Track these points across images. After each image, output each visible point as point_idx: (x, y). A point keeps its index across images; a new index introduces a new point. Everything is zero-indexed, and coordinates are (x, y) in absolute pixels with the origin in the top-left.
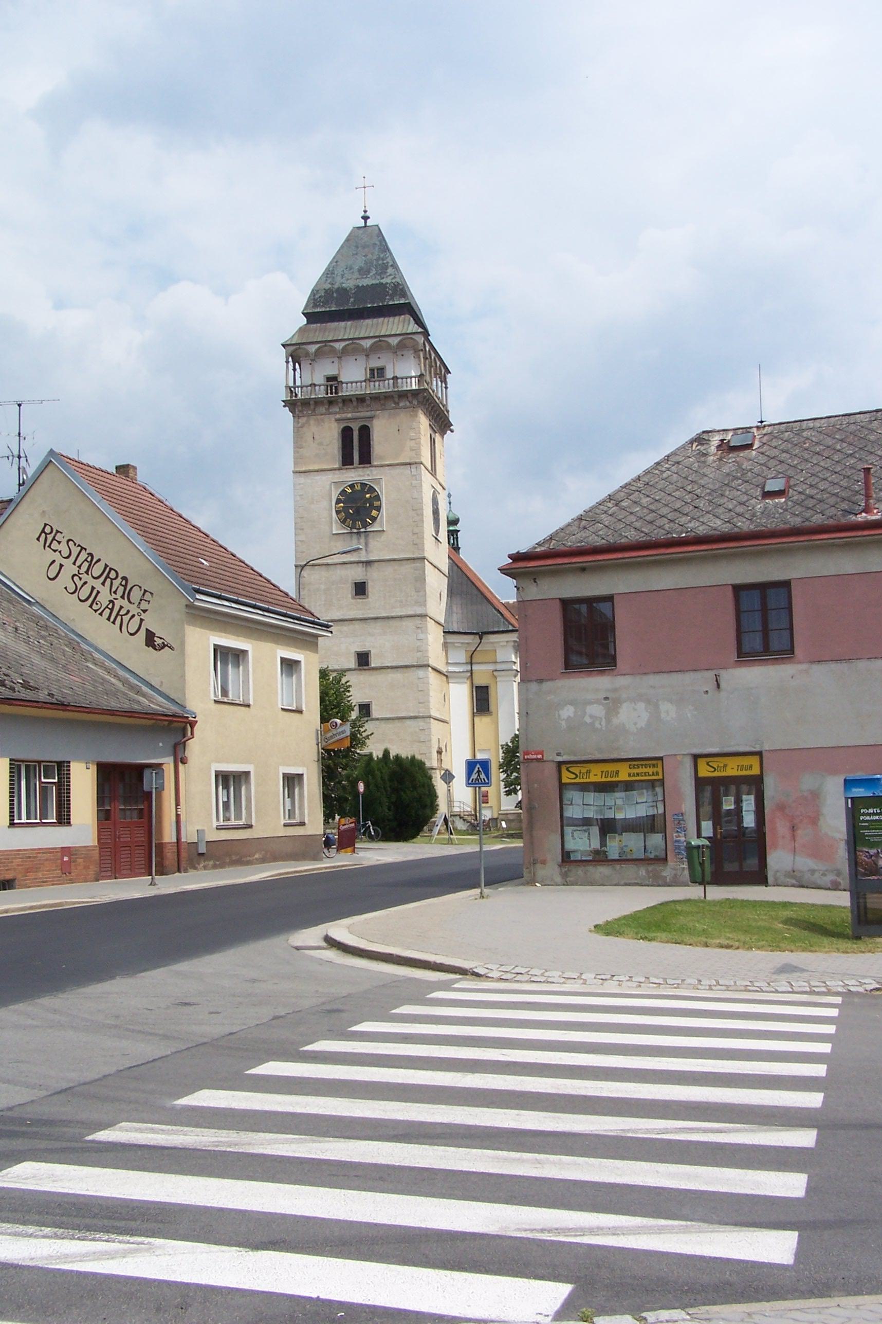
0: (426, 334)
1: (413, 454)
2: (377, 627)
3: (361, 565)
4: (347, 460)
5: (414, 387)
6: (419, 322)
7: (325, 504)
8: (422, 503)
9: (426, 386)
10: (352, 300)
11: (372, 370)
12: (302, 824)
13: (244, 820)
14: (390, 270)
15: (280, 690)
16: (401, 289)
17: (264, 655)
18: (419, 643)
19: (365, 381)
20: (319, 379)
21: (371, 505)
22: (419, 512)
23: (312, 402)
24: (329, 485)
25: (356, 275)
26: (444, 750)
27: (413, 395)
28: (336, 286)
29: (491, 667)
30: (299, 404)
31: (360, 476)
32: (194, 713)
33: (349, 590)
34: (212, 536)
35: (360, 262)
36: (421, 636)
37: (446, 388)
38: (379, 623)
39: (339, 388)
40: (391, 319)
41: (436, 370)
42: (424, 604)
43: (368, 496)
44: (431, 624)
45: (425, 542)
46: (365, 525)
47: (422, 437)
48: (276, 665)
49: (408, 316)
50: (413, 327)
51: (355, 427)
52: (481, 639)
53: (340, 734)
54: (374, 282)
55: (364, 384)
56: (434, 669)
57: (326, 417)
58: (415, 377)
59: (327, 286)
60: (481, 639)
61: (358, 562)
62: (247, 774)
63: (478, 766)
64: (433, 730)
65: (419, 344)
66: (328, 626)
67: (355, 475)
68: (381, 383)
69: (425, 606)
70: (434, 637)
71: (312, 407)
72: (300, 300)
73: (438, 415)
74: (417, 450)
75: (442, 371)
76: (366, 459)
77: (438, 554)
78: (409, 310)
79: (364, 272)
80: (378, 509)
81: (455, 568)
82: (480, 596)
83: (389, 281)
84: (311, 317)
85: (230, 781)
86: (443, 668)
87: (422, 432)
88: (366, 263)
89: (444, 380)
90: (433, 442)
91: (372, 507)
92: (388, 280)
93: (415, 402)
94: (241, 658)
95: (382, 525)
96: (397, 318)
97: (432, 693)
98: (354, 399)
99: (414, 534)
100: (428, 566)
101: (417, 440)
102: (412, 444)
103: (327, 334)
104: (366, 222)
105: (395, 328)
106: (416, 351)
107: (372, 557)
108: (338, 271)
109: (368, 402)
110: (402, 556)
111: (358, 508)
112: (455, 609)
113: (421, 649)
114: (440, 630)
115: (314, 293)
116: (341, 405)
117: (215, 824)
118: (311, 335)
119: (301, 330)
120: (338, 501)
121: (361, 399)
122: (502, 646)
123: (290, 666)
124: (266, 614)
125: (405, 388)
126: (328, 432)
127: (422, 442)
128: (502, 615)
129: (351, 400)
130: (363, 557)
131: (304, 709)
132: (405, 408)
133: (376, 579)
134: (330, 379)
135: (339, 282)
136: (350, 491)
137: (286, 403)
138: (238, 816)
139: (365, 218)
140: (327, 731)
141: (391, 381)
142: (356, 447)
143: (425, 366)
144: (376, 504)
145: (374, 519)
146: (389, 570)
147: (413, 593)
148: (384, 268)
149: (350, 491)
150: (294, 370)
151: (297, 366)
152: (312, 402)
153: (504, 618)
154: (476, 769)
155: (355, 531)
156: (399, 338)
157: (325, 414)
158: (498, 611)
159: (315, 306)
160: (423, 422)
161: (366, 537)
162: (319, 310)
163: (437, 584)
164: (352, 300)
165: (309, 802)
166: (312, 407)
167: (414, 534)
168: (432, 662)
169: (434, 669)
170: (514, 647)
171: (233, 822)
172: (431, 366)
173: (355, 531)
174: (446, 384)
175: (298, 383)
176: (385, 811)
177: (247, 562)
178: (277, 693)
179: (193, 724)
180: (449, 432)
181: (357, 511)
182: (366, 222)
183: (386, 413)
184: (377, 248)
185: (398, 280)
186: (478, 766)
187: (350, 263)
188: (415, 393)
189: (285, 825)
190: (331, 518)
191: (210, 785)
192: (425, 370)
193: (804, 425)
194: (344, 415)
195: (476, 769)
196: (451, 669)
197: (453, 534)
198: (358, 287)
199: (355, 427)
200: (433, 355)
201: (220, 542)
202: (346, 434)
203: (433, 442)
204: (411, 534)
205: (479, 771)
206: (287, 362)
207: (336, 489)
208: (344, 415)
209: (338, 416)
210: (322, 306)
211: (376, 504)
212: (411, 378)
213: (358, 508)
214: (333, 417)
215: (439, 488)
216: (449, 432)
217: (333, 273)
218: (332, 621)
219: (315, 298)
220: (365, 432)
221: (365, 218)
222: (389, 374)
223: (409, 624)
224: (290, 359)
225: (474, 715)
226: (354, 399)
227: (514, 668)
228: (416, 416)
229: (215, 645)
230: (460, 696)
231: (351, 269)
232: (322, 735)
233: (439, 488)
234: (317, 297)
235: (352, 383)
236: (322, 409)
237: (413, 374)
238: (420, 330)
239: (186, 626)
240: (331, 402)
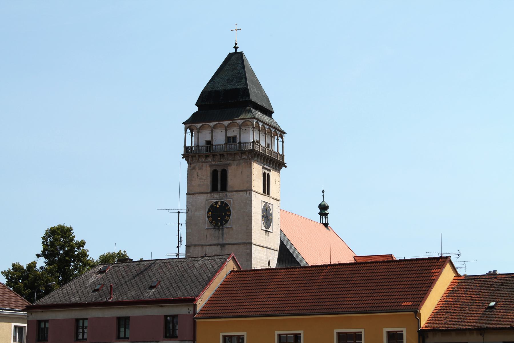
3: (219, 246)
4: (214, 189)
10: (221, 98)
14: (244, 80)
24: (204, 201)
27: (249, 153)
51: (219, 169)
57: (205, 164)
61: (218, 245)
67: (217, 197)
71: (197, 158)
76: (224, 188)
79: (230, 81)
80: (229, 216)
83: (241, 87)
104: (236, 50)
107: (224, 242)
109: (226, 156)
110: (240, 241)
120: (209, 211)
130: (221, 242)
136: (210, 213)
139: (236, 48)
142: (219, 181)
145: (227, 221)
149: (210, 213)
150: (192, 136)
156: (243, 121)
157: (204, 162)
161: (223, 231)
162: (204, 103)
164: (221, 98)
173: (217, 227)
180: (284, 167)
182: (236, 50)
183: (236, 162)
190: (205, 220)
193: (158, 261)
198: (225, 90)
199: (219, 169)
200: (267, 127)
202: (214, 173)
209: (266, 118)
211: (228, 213)
216: (284, 167)
220: (224, 173)
221: (236, 48)
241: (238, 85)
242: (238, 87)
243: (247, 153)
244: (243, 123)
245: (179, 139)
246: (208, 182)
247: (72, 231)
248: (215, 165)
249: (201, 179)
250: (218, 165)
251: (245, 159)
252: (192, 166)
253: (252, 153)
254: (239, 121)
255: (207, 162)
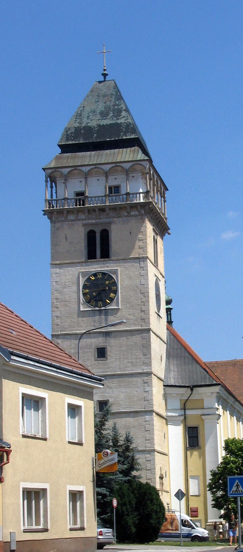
0: (150, 161)
1: (141, 251)
2: (114, 383)
4: (91, 255)
5: (142, 201)
6: (145, 152)
7: (75, 288)
8: (148, 288)
9: (151, 200)
11: (110, 188)
12: (82, 529)
13: (42, 524)
14: (124, 113)
15: (68, 428)
16: (133, 128)
17: (57, 402)
18: (146, 394)
19: (105, 196)
20: (69, 193)
21: (110, 289)
22: (145, 294)
23: (65, 212)
25: (98, 117)
26: (164, 476)
28: (83, 125)
29: (200, 412)
30: (55, 213)
31: (101, 267)
32: (9, 445)
33: (93, 353)
34: (15, 313)
35: (101, 107)
36: (147, 389)
37: (165, 201)
38: (115, 380)
39: (86, 200)
40: (125, 150)
41: (157, 188)
42: (149, 364)
43: (107, 282)
44: (155, 380)
45: (151, 317)
46: (105, 304)
47: (148, 238)
48: (64, 409)
49: (137, 148)
50: (141, 156)
52: (192, 390)
53: (111, 460)
54: (112, 122)
55: (104, 198)
56: (158, 414)
58: (142, 193)
59: (77, 125)
60: (192, 390)
62: (45, 490)
63: (237, 481)
64: (157, 461)
65: (147, 169)
66: (100, 380)
68: (117, 197)
69: (151, 365)
70: (157, 390)
71: (65, 215)
72: (57, 136)
73: (159, 221)
74: (144, 248)
75: (162, 188)
76: (106, 254)
77: (158, 325)
78: (137, 142)
79: (104, 115)
80: (115, 292)
81: (172, 337)
82: (190, 358)
84: (65, 149)
85: (33, 496)
86: (163, 413)
87: (148, 234)
88: (105, 108)
89: (163, 196)
90: (155, 241)
91: (111, 291)
92: (122, 121)
93: (143, 212)
94: (40, 403)
95: (117, 305)
96: (129, 149)
97: (156, 432)
98: (97, 210)
99: (142, 311)
100: (152, 336)
101: (144, 241)
102: (141, 244)
103: (76, 160)
104: (105, 78)
105: (128, 156)
106: (144, 174)
108: (85, 114)
111: (100, 292)
112: (172, 368)
113: (149, 400)
114: (161, 383)
115: (67, 130)
116: (87, 214)
117: (22, 528)
118: (65, 161)
119: (57, 158)
120: (85, 287)
121: (102, 210)
122: (209, 396)
123: (74, 410)
124: (58, 371)
125: (135, 202)
126: (77, 234)
127: (148, 242)
128: (207, 372)
129: (95, 210)
131: (84, 442)
132: (135, 216)
133: (114, 347)
134: (78, 194)
135: (85, 122)
136: (93, 278)
137: (45, 212)
138: (38, 523)
139: (105, 75)
140: (100, 458)
141: (125, 196)
142: (98, 246)
143: (150, 184)
144: (114, 288)
145: (112, 300)
146: (123, 340)
147: (141, 356)
148: (120, 111)
149: (93, 278)
150: (52, 187)
151: (54, 185)
152: (65, 212)
153: (210, 375)
154: (236, 484)
155: (97, 308)
156: (131, 164)
158: (205, 369)
159: (68, 139)
160: (149, 228)
162: (70, 143)
163: (158, 348)
164: (95, 135)
165: (87, 513)
166: (65, 215)
167: (142, 311)
168: (156, 409)
169: (158, 414)
170: (217, 397)
171: (34, 527)
172: (154, 185)
174: (164, 198)
175: (54, 198)
176: (131, 520)
177: (41, 332)
178: (65, 430)
179: (8, 453)
181: (99, 294)
182: (105, 78)
184: (113, 97)
185: (130, 121)
186: (237, 481)
187: (93, 108)
188: (142, 205)
189: (71, 530)
191: (19, 498)
192: (150, 188)
194: (90, 221)
195: (236, 484)
196: (170, 414)
197: (168, 310)
201: (21, 318)
202: (91, 236)
203: (155, 241)
204: (139, 311)
205: (237, 485)
206: (46, 181)
207: (83, 277)
208: (90, 221)
209: (85, 222)
210: (72, 140)
211: (114, 288)
212: (140, 193)
213: (100, 292)
214: (80, 223)
215: (160, 277)
216: (167, 234)
217: (80, 115)
218: (105, 376)
219: (67, 135)
220: (105, 235)
221: (105, 75)
222: (123, 191)
223: (139, 380)
224: (49, 180)
225: (186, 449)
226: (97, 210)
227: (217, 413)
228: (144, 222)
229: (23, 394)
230: (176, 435)
231: (94, 112)
232: (96, 461)
233: (160, 277)
234: (69, 132)
235: (95, 197)
236: (71, 217)
237: (141, 191)
238: (146, 158)
239: (3, 380)
240: (79, 211)
241: (118, 119)
242: (119, 121)
243: (139, 207)
244: (132, 166)
245: (40, 194)
246: (82, 245)
247: (214, 502)
248: (92, 224)
249: (71, 243)
250: (96, 224)
251: (135, 216)
252: (58, 225)
253: (147, 207)
254: (126, 164)
255: (79, 220)
